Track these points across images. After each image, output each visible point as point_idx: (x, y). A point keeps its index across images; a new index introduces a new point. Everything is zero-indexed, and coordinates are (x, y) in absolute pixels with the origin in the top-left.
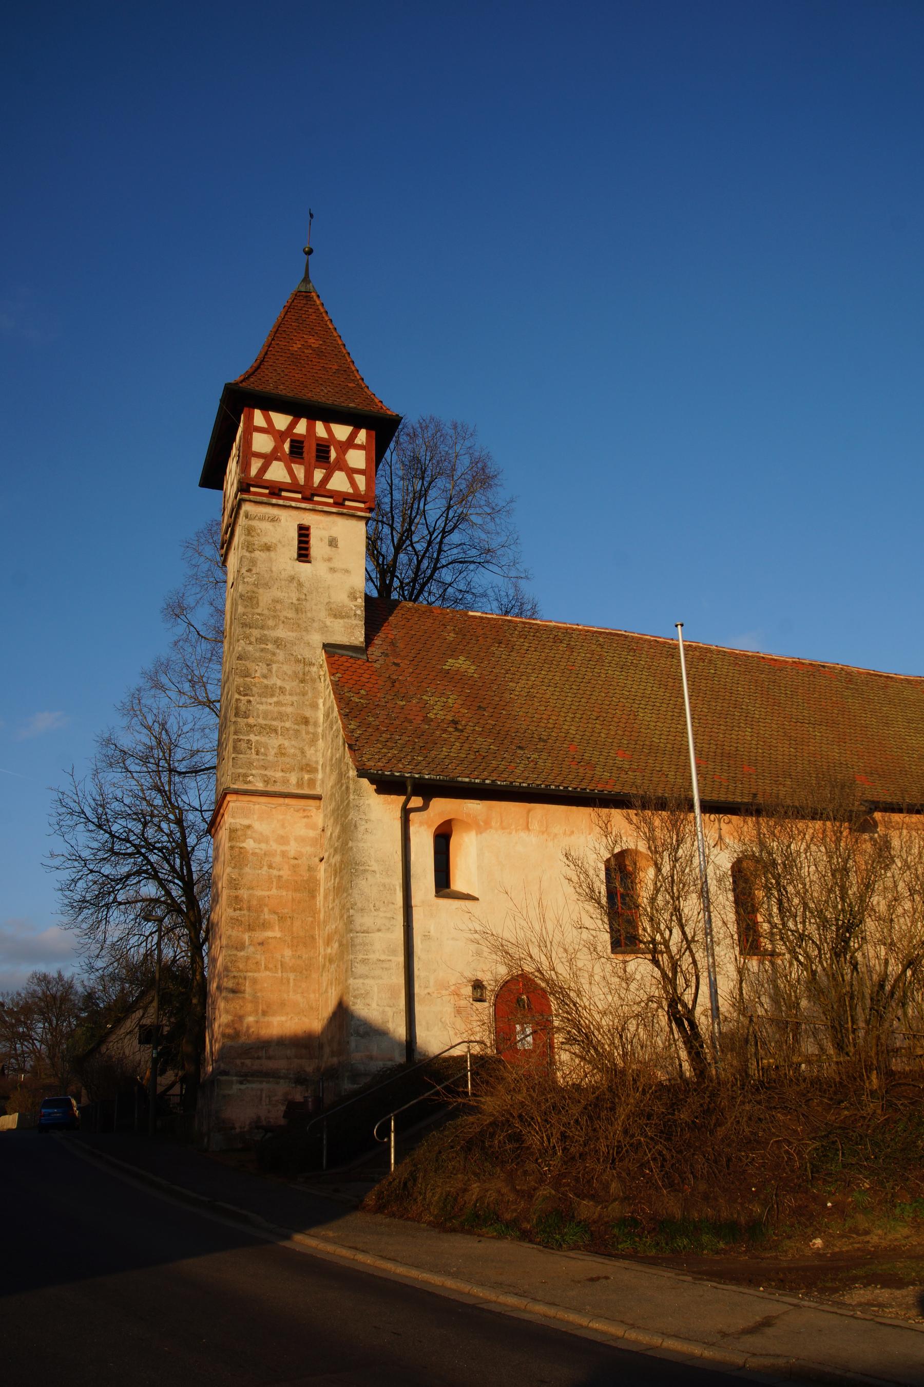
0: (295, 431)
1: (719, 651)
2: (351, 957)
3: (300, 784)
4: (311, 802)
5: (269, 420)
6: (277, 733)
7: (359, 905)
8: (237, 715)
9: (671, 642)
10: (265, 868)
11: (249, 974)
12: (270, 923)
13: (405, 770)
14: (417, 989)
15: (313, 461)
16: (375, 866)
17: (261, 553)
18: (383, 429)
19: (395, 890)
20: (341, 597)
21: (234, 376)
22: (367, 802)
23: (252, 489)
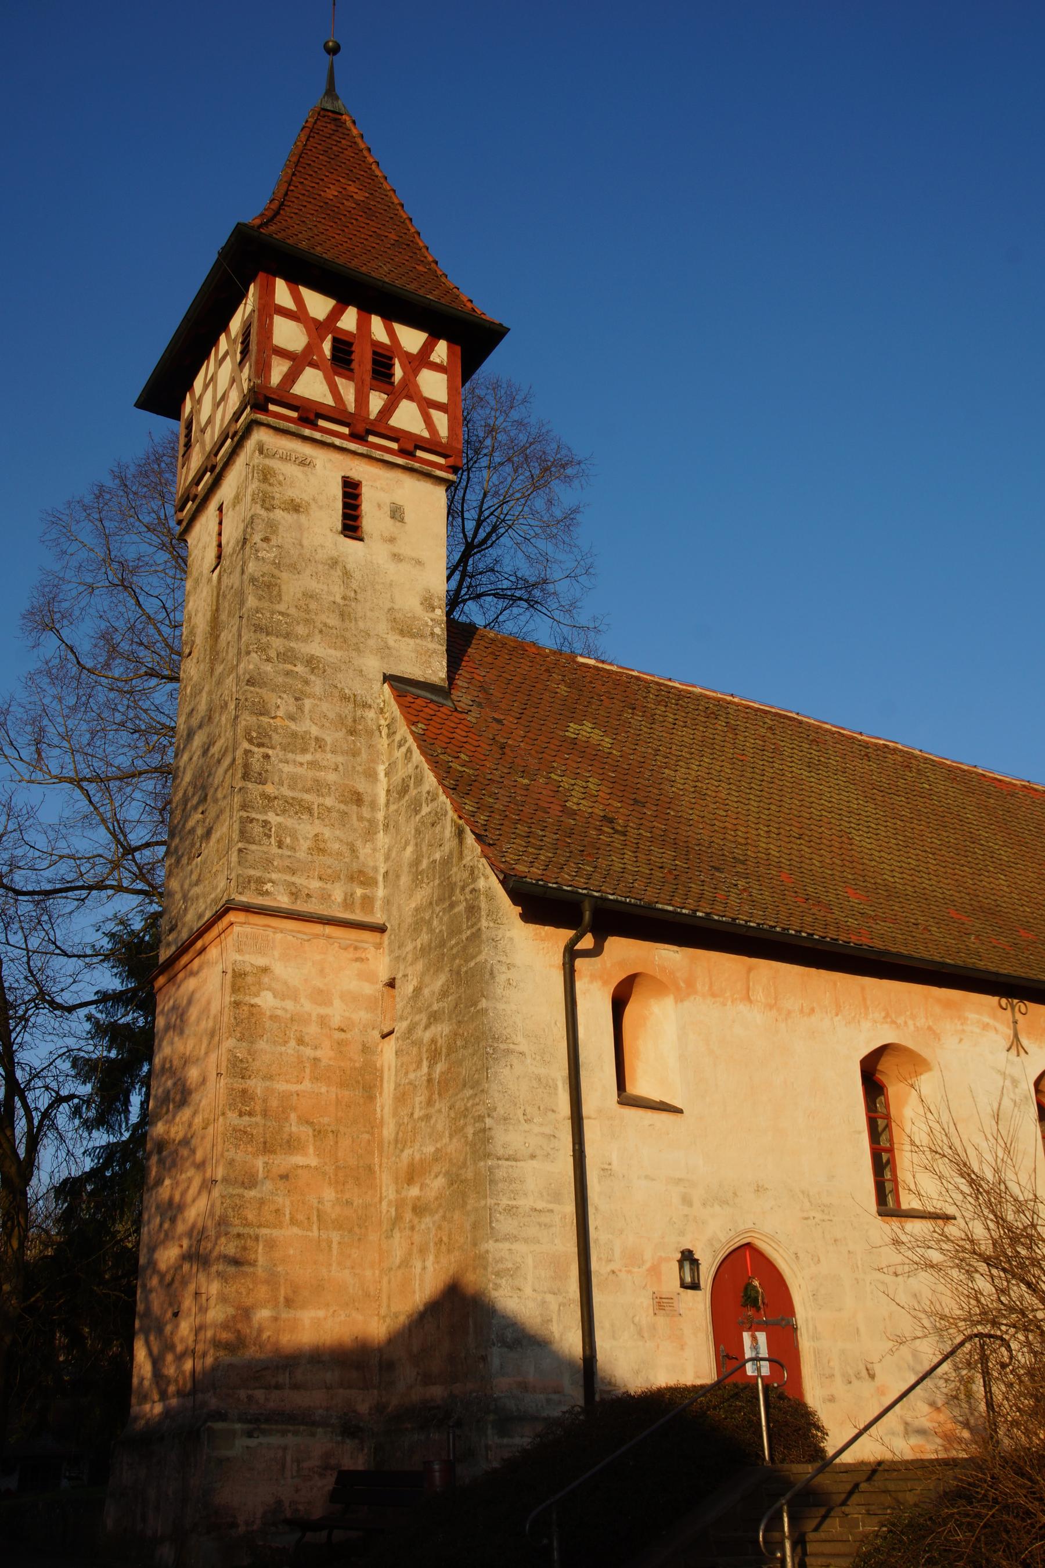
0: (339, 324)
1: (926, 759)
2: (490, 1202)
3: (348, 903)
4: (366, 935)
6: (311, 814)
7: (501, 1111)
8: (246, 777)
9: (860, 737)
10: (293, 1043)
11: (264, 1231)
12: (299, 1139)
13: (568, 879)
14: (594, 1265)
15: (368, 377)
16: (523, 1046)
17: (285, 514)
18: (473, 340)
19: (556, 1088)
20: (410, 603)
21: (250, 216)
22: (508, 934)
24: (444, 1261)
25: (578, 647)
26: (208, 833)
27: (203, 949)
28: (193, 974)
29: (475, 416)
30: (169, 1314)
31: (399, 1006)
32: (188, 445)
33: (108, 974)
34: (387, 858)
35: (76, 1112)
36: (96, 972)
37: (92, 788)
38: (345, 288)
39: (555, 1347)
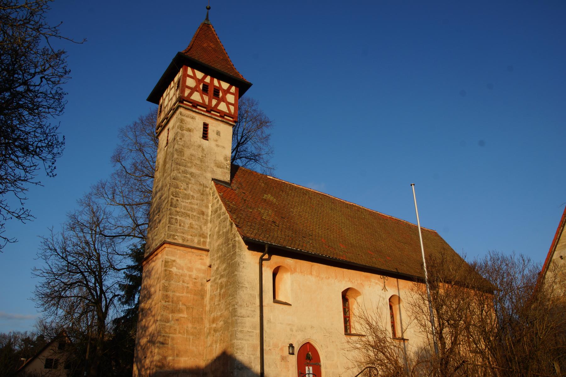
2: (236, 329)
3: (199, 243)
4: (204, 252)
5: (194, 73)
7: (240, 303)
8: (171, 206)
10: (181, 282)
11: (171, 335)
13: (262, 239)
15: (212, 95)
18: (242, 87)
20: (221, 159)
21: (182, 50)
23: (185, 102)
24: (222, 345)
25: (268, 173)
26: (160, 222)
27: (157, 254)
28: (153, 261)
29: (242, 107)
30: (143, 357)
31: (212, 273)
32: (161, 112)
33: (130, 260)
34: (210, 231)
35: (120, 299)
36: (127, 260)
37: (128, 207)
38: (207, 70)
39: (252, 370)
